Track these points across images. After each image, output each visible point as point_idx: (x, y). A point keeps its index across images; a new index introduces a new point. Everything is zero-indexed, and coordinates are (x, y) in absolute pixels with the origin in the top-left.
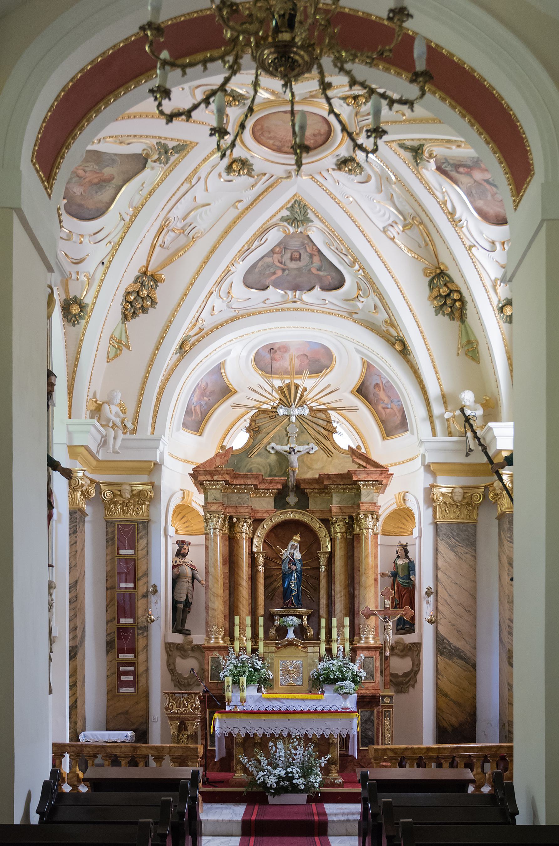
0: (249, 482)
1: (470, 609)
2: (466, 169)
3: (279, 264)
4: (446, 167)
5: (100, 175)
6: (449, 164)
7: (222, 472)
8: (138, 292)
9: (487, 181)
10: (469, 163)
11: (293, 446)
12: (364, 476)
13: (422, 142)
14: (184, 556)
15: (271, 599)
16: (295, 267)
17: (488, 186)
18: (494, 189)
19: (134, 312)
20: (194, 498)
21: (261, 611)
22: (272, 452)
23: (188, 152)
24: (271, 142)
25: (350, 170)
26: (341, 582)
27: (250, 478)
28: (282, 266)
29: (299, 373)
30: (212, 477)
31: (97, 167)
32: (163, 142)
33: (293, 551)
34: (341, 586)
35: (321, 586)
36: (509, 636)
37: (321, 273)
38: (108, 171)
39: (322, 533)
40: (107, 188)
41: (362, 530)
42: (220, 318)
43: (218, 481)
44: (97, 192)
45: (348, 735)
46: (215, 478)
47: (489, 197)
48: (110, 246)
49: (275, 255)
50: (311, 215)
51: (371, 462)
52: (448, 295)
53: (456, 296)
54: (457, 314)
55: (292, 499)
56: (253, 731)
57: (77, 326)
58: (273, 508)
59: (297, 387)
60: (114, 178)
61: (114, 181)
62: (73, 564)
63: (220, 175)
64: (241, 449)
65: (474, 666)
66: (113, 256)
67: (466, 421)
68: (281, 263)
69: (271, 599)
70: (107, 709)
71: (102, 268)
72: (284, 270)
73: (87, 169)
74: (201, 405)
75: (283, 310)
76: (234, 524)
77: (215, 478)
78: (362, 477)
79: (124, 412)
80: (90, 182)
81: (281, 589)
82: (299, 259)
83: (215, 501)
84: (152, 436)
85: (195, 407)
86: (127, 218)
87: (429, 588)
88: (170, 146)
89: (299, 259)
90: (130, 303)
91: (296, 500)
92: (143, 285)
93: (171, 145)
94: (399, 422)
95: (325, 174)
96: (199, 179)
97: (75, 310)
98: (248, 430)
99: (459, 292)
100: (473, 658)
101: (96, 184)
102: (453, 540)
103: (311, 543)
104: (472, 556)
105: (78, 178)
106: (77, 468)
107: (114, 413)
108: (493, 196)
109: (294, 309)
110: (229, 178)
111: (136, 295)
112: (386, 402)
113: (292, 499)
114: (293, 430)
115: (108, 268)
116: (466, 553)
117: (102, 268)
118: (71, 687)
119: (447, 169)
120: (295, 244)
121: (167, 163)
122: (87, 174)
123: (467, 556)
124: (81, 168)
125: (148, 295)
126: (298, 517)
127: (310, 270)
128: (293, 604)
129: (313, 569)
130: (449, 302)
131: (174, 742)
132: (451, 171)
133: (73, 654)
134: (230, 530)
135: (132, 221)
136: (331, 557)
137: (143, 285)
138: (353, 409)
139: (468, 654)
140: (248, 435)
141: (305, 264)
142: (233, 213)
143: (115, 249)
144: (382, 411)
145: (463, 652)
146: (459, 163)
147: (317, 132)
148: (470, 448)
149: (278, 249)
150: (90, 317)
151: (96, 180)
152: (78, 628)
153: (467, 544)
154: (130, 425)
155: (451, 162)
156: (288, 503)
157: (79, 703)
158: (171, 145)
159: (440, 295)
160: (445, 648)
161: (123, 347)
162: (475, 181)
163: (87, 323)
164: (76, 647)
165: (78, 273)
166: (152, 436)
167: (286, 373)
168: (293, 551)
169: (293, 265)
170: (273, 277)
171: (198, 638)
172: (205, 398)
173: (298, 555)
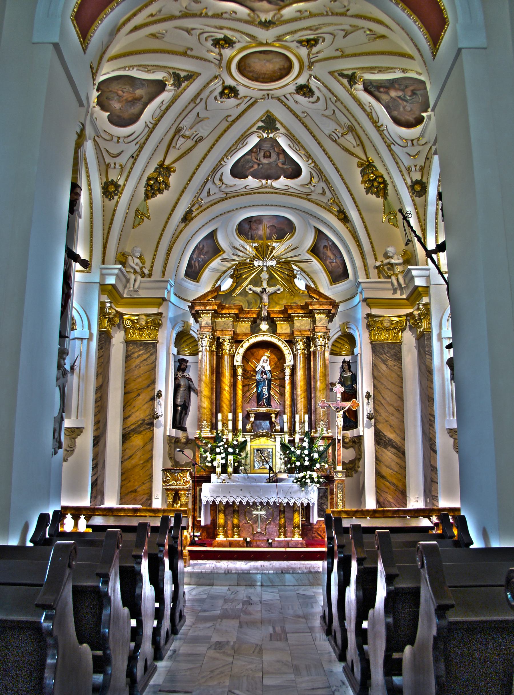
0: (232, 312)
1: (399, 409)
2: (385, 90)
3: (255, 160)
4: (371, 88)
5: (133, 95)
6: (373, 86)
7: (213, 303)
8: (156, 179)
9: (399, 97)
10: (387, 85)
12: (318, 306)
13: (354, 71)
14: (184, 370)
15: (248, 402)
16: (267, 162)
17: (400, 101)
18: (405, 103)
19: (153, 193)
20: (192, 328)
22: (251, 292)
23: (194, 80)
24: (251, 74)
25: (304, 93)
26: (301, 387)
27: (233, 309)
28: (257, 161)
29: (269, 238)
30: (205, 308)
31: (131, 89)
32: (177, 72)
33: (264, 362)
34: (301, 390)
35: (286, 391)
36: (431, 428)
37: (285, 167)
38: (139, 92)
39: (286, 350)
40: (138, 104)
41: (317, 346)
43: (209, 310)
44: (131, 107)
45: (308, 504)
46: (207, 308)
47: (401, 109)
48: (138, 145)
49: (253, 154)
50: (278, 126)
51: (322, 295)
52: (375, 179)
53: (380, 180)
54: (381, 193)
55: (264, 326)
57: (112, 200)
58: (250, 332)
59: (268, 246)
60: (142, 97)
61: (143, 100)
62: (99, 372)
63: (216, 98)
64: (228, 290)
65: (404, 453)
66: (140, 152)
67: (403, 219)
68: (257, 159)
69: (248, 402)
70: (121, 488)
71: (131, 160)
72: (259, 165)
73: (125, 90)
74: (199, 261)
75: (258, 193)
76: (221, 343)
77: (207, 308)
78: (316, 307)
79: (143, 263)
80: (126, 100)
81: (256, 394)
82: (270, 157)
83: (207, 326)
84: (163, 279)
85: (195, 262)
86: (151, 126)
87: (368, 393)
88: (182, 75)
89: (270, 157)
90: (151, 186)
91: (267, 327)
92: (160, 173)
93: (183, 74)
94: (341, 272)
95: (288, 96)
96: (201, 99)
97: (112, 188)
98: (232, 276)
99: (382, 177)
100: (403, 447)
101: (130, 101)
102: (385, 356)
104: (399, 368)
105: (118, 97)
106: (107, 301)
107: (135, 263)
108: (404, 108)
109: (266, 193)
110: (222, 100)
111: (155, 180)
112: (332, 258)
113: (264, 326)
114: (265, 276)
115: (136, 160)
116: (395, 366)
117: (131, 160)
118: (93, 468)
119: (372, 90)
120: (266, 146)
121: (180, 87)
122: (124, 94)
123: (395, 367)
124: (121, 89)
125: (163, 181)
127: (277, 164)
128: (264, 405)
129: (280, 379)
130: (375, 184)
132: (375, 91)
133: (95, 442)
135: (154, 128)
136: (294, 369)
137: (160, 173)
138: (307, 261)
139: (399, 444)
140: (232, 280)
141: (274, 160)
142: (225, 124)
143: (141, 147)
144: (329, 265)
145: (395, 442)
146: (380, 85)
147: (282, 67)
148: (408, 239)
149: (255, 150)
150: (121, 194)
151: (130, 99)
152: (101, 422)
153: (395, 359)
155: (375, 84)
156: (261, 330)
157: (99, 482)
158: (183, 74)
159: (369, 180)
160: (381, 439)
161: (145, 218)
162: (391, 98)
163: (119, 198)
164: (98, 436)
165: (115, 164)
166: (163, 279)
167: (261, 238)
168: (264, 362)
169: (265, 161)
170: (251, 170)
171: (192, 432)
172: (202, 256)
173: (268, 368)
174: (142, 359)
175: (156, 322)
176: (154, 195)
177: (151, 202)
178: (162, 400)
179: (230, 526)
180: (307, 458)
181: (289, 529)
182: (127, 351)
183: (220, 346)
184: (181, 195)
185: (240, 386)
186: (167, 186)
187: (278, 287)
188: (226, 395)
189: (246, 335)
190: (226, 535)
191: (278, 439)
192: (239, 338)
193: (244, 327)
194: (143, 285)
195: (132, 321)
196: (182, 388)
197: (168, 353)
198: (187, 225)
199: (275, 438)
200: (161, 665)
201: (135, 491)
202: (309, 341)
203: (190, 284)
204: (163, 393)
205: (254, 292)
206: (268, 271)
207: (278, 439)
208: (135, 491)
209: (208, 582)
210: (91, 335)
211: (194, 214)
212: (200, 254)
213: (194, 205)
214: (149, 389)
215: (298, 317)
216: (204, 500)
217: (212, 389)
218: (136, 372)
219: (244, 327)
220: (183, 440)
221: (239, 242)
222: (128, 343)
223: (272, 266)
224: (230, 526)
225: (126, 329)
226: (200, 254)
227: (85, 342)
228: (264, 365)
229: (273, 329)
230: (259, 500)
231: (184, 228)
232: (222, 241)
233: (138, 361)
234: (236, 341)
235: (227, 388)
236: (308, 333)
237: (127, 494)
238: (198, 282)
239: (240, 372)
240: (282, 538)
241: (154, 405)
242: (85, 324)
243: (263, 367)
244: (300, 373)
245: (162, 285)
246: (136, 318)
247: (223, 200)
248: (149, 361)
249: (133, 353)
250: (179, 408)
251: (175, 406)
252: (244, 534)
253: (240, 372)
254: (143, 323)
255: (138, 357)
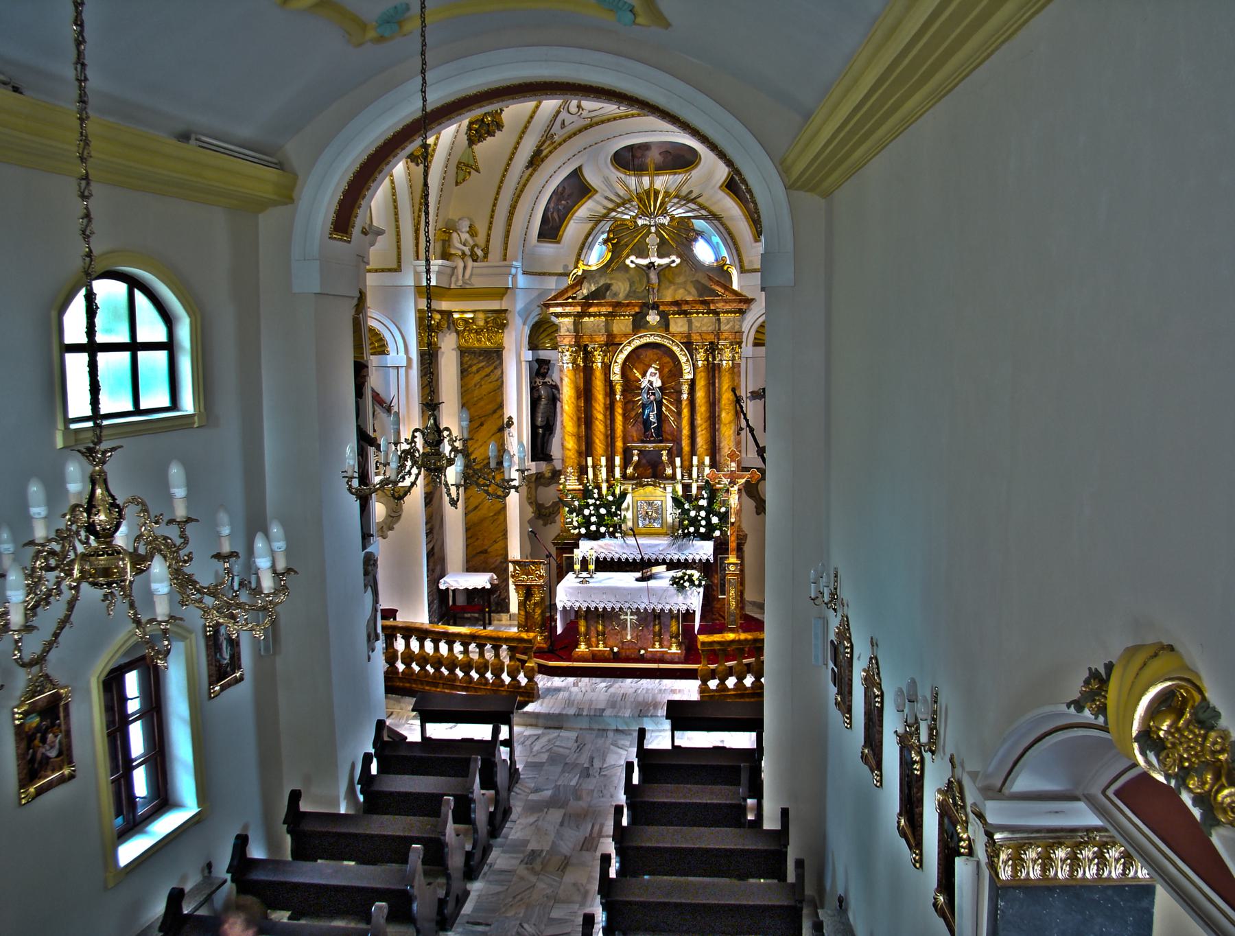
11: (653, 260)
14: (544, 376)
21: (619, 444)
22: (632, 266)
42: (570, 129)
55: (653, 318)
56: (625, 556)
74: (559, 210)
103: (672, 373)
118: (427, 534)
126: (658, 340)
131: (428, 692)
134: (585, 360)
136: (692, 384)
154: (479, 253)
157: (436, 550)
168: (652, 378)
174: (483, 373)
175: (498, 321)
176: (481, 138)
177: (479, 148)
178: (514, 430)
179: (593, 633)
180: (703, 523)
181: (666, 637)
182: (462, 364)
183: (588, 357)
184: (521, 138)
185: (619, 410)
186: (499, 126)
187: (673, 257)
188: (599, 427)
189: (626, 336)
190: (589, 645)
191: (669, 489)
192: (617, 340)
193: (622, 325)
194: (475, 271)
195: (466, 321)
196: (543, 401)
197: (519, 363)
198: (535, 170)
199: (665, 488)
200: (476, 887)
201: (485, 552)
202: (712, 349)
203: (548, 249)
204: (515, 420)
205: (637, 265)
206: (657, 232)
207: (669, 489)
208: (485, 552)
209: (557, 725)
210: (409, 360)
211: (544, 153)
212: (559, 200)
213: (544, 142)
214: (496, 416)
215: (698, 313)
216: (560, 606)
217: (579, 419)
218: (476, 393)
219: (622, 325)
220: (548, 475)
221: (615, 174)
222: (463, 352)
223: (663, 225)
224: (593, 633)
225: (458, 332)
226: (559, 200)
227: (402, 371)
228: (652, 379)
229: (665, 324)
230: (627, 605)
231: (531, 175)
232: (591, 177)
233: (477, 378)
234: (612, 344)
235: (600, 417)
236: (711, 338)
237: (474, 556)
238: (559, 242)
239: (618, 388)
240: (657, 648)
241: (503, 438)
242: (402, 348)
243: (651, 383)
244: (700, 394)
245: (503, 270)
246: (471, 316)
247: (586, 129)
248: (493, 377)
249: (471, 366)
250: (541, 431)
251: (534, 427)
252: (611, 642)
253: (618, 388)
254: (481, 323)
255: (478, 371)
